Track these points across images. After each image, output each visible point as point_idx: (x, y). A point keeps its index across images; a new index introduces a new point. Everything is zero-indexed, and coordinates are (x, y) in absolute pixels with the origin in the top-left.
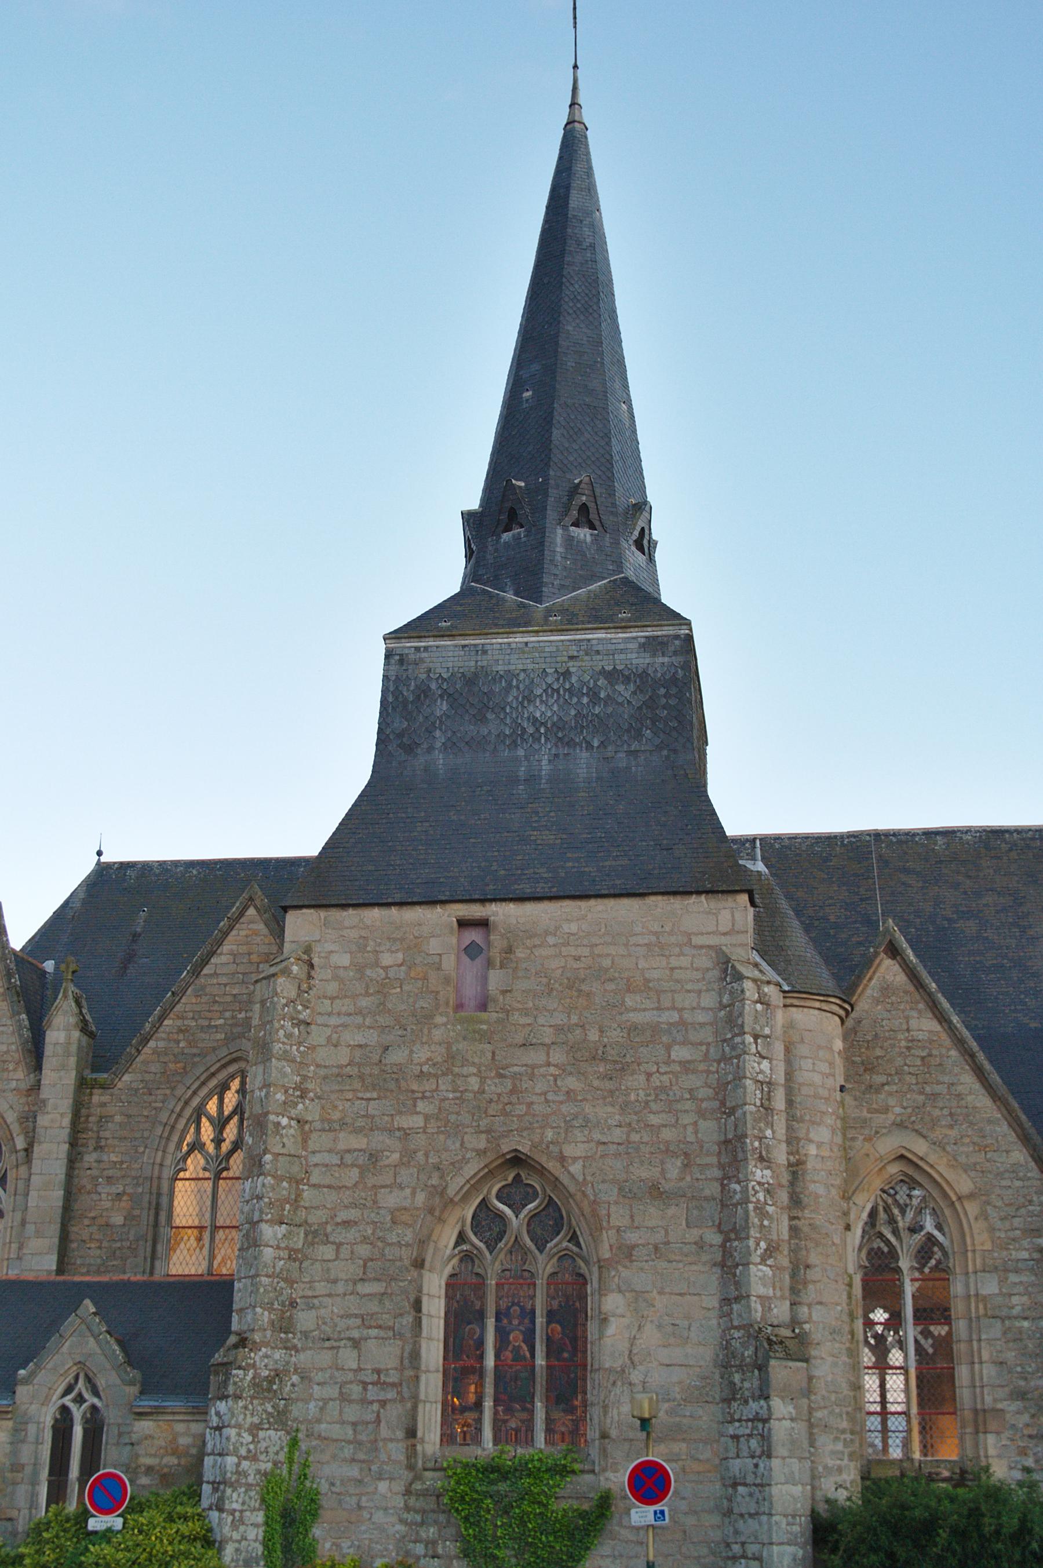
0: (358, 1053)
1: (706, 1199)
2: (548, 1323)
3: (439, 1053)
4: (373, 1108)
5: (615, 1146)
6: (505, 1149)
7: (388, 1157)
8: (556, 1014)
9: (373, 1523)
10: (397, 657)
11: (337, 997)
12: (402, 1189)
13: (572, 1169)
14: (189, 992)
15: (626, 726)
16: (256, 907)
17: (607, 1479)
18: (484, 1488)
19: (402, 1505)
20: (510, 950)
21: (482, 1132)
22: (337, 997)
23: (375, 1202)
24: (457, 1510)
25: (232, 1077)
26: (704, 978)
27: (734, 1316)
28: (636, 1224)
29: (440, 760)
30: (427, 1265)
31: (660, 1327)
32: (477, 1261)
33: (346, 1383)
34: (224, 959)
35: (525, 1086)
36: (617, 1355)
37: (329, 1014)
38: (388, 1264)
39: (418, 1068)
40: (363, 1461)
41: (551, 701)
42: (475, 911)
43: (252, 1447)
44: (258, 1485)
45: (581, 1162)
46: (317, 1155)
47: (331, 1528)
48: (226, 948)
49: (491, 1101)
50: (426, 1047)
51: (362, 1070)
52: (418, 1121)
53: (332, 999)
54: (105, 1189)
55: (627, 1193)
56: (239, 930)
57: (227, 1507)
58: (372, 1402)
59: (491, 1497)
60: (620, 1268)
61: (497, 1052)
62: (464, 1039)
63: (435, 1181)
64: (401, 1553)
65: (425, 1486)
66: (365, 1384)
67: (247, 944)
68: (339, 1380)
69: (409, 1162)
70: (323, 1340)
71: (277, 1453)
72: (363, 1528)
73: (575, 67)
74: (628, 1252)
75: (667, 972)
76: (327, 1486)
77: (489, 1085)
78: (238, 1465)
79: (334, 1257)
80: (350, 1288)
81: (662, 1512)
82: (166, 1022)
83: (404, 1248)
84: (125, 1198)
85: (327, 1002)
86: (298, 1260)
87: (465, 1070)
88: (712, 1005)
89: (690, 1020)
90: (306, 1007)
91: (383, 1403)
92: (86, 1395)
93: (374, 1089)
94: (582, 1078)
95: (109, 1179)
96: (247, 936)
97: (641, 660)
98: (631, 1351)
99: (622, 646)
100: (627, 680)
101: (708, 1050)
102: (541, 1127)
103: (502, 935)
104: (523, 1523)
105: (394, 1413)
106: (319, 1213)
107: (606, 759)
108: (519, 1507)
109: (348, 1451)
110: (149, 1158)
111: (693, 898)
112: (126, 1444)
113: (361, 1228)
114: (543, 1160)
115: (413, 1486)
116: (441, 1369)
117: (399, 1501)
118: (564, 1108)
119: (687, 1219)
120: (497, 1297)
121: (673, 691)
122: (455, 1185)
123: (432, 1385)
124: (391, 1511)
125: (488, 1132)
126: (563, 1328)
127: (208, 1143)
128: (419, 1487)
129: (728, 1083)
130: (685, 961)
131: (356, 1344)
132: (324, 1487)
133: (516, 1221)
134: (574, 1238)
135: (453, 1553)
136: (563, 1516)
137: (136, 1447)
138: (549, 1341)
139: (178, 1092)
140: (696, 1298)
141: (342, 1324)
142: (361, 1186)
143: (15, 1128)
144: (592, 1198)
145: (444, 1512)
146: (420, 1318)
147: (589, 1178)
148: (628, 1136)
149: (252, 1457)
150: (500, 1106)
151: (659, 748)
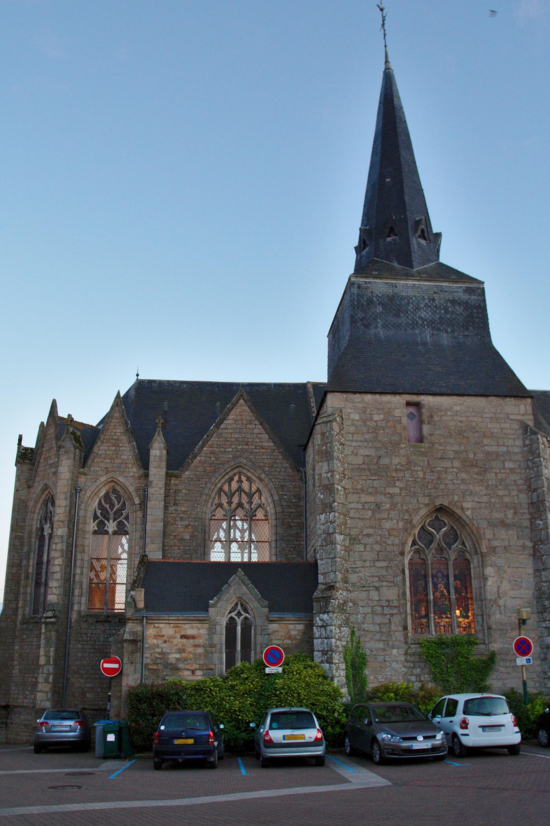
0: (366, 459)
2: (455, 580)
3: (404, 460)
8: (454, 445)
10: (357, 285)
11: (355, 433)
12: (392, 520)
13: (467, 513)
14: (214, 436)
15: (461, 324)
16: (244, 399)
17: (492, 646)
19: (404, 659)
20: (431, 416)
22: (355, 433)
23: (380, 526)
24: (430, 661)
25: (235, 475)
27: (543, 577)
28: (496, 538)
29: (381, 332)
31: (509, 581)
32: (422, 553)
33: (374, 606)
34: (230, 422)
37: (352, 441)
38: (388, 553)
39: (395, 467)
40: (385, 641)
41: (428, 311)
42: (414, 398)
43: (339, 634)
44: (342, 652)
46: (352, 504)
47: (373, 670)
48: (230, 417)
49: (429, 482)
50: (398, 458)
51: (369, 467)
52: (398, 490)
53: (353, 434)
54: (179, 523)
55: (491, 524)
56: (236, 409)
57: (334, 661)
58: (386, 614)
59: (444, 655)
61: (430, 461)
63: (406, 517)
66: (383, 607)
67: (241, 415)
71: (347, 638)
73: (385, 46)
74: (493, 550)
75: (500, 430)
78: (336, 642)
80: (372, 564)
81: (529, 659)
82: (204, 449)
84: (189, 527)
85: (350, 435)
87: (416, 469)
89: (511, 451)
90: (343, 437)
91: (392, 615)
92: (242, 613)
95: (181, 518)
96: (240, 412)
97: (465, 297)
98: (498, 592)
99: (455, 290)
100: (460, 304)
101: (520, 465)
103: (428, 410)
104: (459, 665)
105: (397, 619)
106: (355, 530)
107: (455, 338)
109: (378, 636)
110: (200, 509)
111: (508, 399)
112: (265, 634)
114: (454, 509)
117: (403, 658)
118: (461, 487)
121: (480, 311)
125: (429, 496)
127: (225, 504)
129: (531, 478)
130: (507, 426)
131: (377, 589)
132: (368, 652)
134: (463, 544)
137: (270, 636)
138: (456, 588)
139: (213, 480)
142: (373, 519)
143: (134, 494)
145: (423, 662)
147: (475, 517)
148: (490, 499)
149: (340, 639)
151: (477, 334)
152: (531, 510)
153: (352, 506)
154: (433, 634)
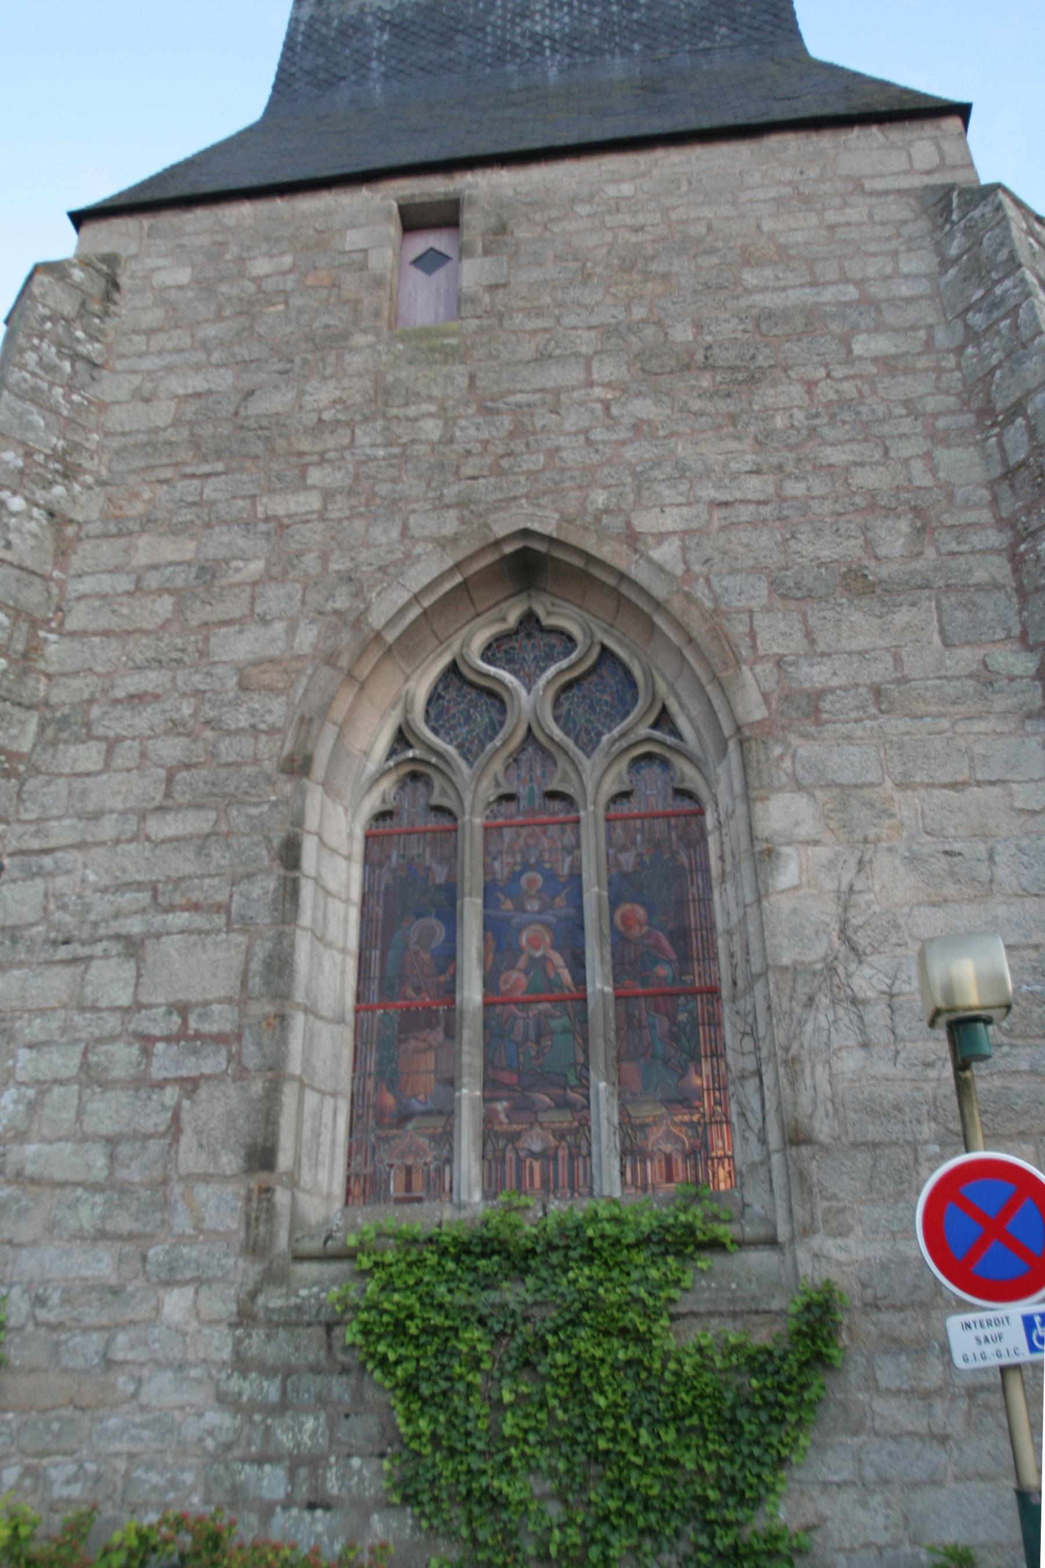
0: (190, 409)
1: (979, 587)
2: (615, 902)
4: (211, 490)
5: (751, 508)
6: (501, 530)
7: (238, 570)
9: (143, 1408)
13: (656, 554)
18: (460, 1298)
19: (226, 1354)
20: (502, 229)
21: (448, 507)
23: (203, 654)
26: (899, 235)
28: (821, 647)
30: (319, 769)
31: (913, 860)
33: (100, 1041)
35: (539, 423)
36: (809, 931)
37: (141, 355)
38: (224, 773)
40: (130, 1237)
45: (676, 542)
46: (87, 579)
50: (332, 383)
55: (789, 591)
58: (162, 1085)
59: (482, 1321)
60: (793, 739)
62: (411, 362)
63: (341, 601)
64: (219, 1495)
65: (293, 1300)
66: (147, 1041)
68: (84, 1035)
69: (285, 573)
70: (54, 943)
72: (113, 1423)
74: (811, 706)
76: (25, 1307)
77: (462, 429)
79: (100, 766)
83: (263, 738)
86: (17, 775)
87: (412, 411)
88: (924, 269)
89: (882, 295)
91: (191, 1085)
93: (219, 458)
94: (664, 399)
98: (844, 923)
102: (580, 487)
105: (219, 1108)
106: (76, 683)
108: (564, 1346)
113: (168, 706)
114: (590, 544)
115: (261, 1300)
116: (350, 1017)
117: (219, 1345)
118: (629, 453)
119: (942, 631)
120: (486, 852)
122: (385, 606)
123: (323, 1047)
124: (194, 1373)
126: (651, 911)
128: (276, 1303)
130: (853, 214)
131: (132, 947)
133: (530, 697)
134: (663, 719)
135: (370, 1493)
136: (701, 1368)
138: (620, 941)
140: (995, 790)
141: (102, 905)
142: (175, 627)
144: (709, 605)
145: (345, 1370)
146: (295, 881)
147: (697, 568)
148: (779, 487)
150: (488, 460)
152: (1009, 506)
153: (86, 585)
154: (469, 1196)
